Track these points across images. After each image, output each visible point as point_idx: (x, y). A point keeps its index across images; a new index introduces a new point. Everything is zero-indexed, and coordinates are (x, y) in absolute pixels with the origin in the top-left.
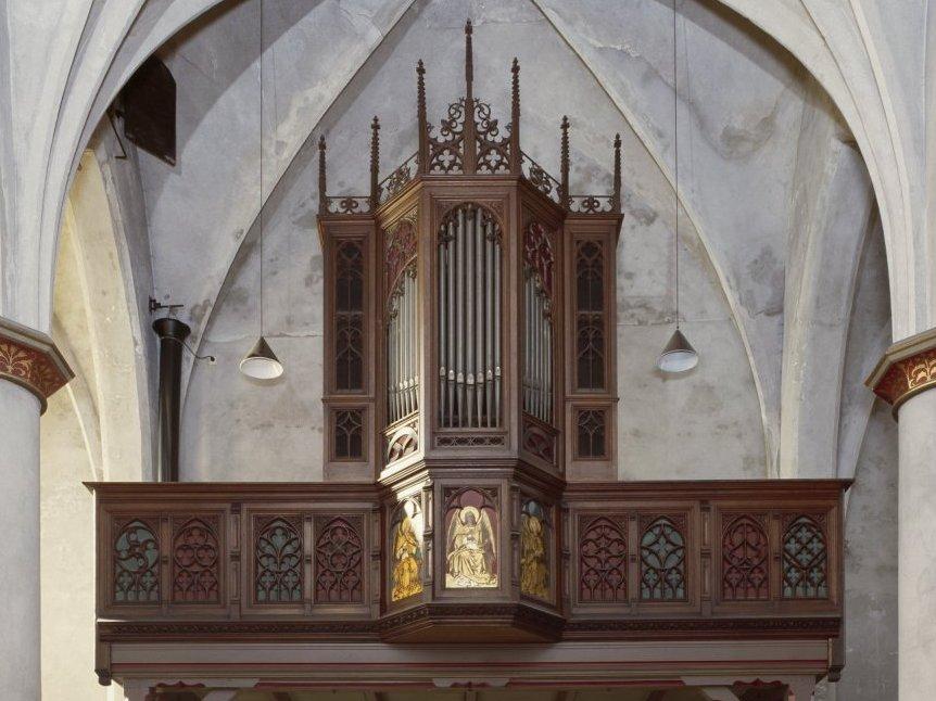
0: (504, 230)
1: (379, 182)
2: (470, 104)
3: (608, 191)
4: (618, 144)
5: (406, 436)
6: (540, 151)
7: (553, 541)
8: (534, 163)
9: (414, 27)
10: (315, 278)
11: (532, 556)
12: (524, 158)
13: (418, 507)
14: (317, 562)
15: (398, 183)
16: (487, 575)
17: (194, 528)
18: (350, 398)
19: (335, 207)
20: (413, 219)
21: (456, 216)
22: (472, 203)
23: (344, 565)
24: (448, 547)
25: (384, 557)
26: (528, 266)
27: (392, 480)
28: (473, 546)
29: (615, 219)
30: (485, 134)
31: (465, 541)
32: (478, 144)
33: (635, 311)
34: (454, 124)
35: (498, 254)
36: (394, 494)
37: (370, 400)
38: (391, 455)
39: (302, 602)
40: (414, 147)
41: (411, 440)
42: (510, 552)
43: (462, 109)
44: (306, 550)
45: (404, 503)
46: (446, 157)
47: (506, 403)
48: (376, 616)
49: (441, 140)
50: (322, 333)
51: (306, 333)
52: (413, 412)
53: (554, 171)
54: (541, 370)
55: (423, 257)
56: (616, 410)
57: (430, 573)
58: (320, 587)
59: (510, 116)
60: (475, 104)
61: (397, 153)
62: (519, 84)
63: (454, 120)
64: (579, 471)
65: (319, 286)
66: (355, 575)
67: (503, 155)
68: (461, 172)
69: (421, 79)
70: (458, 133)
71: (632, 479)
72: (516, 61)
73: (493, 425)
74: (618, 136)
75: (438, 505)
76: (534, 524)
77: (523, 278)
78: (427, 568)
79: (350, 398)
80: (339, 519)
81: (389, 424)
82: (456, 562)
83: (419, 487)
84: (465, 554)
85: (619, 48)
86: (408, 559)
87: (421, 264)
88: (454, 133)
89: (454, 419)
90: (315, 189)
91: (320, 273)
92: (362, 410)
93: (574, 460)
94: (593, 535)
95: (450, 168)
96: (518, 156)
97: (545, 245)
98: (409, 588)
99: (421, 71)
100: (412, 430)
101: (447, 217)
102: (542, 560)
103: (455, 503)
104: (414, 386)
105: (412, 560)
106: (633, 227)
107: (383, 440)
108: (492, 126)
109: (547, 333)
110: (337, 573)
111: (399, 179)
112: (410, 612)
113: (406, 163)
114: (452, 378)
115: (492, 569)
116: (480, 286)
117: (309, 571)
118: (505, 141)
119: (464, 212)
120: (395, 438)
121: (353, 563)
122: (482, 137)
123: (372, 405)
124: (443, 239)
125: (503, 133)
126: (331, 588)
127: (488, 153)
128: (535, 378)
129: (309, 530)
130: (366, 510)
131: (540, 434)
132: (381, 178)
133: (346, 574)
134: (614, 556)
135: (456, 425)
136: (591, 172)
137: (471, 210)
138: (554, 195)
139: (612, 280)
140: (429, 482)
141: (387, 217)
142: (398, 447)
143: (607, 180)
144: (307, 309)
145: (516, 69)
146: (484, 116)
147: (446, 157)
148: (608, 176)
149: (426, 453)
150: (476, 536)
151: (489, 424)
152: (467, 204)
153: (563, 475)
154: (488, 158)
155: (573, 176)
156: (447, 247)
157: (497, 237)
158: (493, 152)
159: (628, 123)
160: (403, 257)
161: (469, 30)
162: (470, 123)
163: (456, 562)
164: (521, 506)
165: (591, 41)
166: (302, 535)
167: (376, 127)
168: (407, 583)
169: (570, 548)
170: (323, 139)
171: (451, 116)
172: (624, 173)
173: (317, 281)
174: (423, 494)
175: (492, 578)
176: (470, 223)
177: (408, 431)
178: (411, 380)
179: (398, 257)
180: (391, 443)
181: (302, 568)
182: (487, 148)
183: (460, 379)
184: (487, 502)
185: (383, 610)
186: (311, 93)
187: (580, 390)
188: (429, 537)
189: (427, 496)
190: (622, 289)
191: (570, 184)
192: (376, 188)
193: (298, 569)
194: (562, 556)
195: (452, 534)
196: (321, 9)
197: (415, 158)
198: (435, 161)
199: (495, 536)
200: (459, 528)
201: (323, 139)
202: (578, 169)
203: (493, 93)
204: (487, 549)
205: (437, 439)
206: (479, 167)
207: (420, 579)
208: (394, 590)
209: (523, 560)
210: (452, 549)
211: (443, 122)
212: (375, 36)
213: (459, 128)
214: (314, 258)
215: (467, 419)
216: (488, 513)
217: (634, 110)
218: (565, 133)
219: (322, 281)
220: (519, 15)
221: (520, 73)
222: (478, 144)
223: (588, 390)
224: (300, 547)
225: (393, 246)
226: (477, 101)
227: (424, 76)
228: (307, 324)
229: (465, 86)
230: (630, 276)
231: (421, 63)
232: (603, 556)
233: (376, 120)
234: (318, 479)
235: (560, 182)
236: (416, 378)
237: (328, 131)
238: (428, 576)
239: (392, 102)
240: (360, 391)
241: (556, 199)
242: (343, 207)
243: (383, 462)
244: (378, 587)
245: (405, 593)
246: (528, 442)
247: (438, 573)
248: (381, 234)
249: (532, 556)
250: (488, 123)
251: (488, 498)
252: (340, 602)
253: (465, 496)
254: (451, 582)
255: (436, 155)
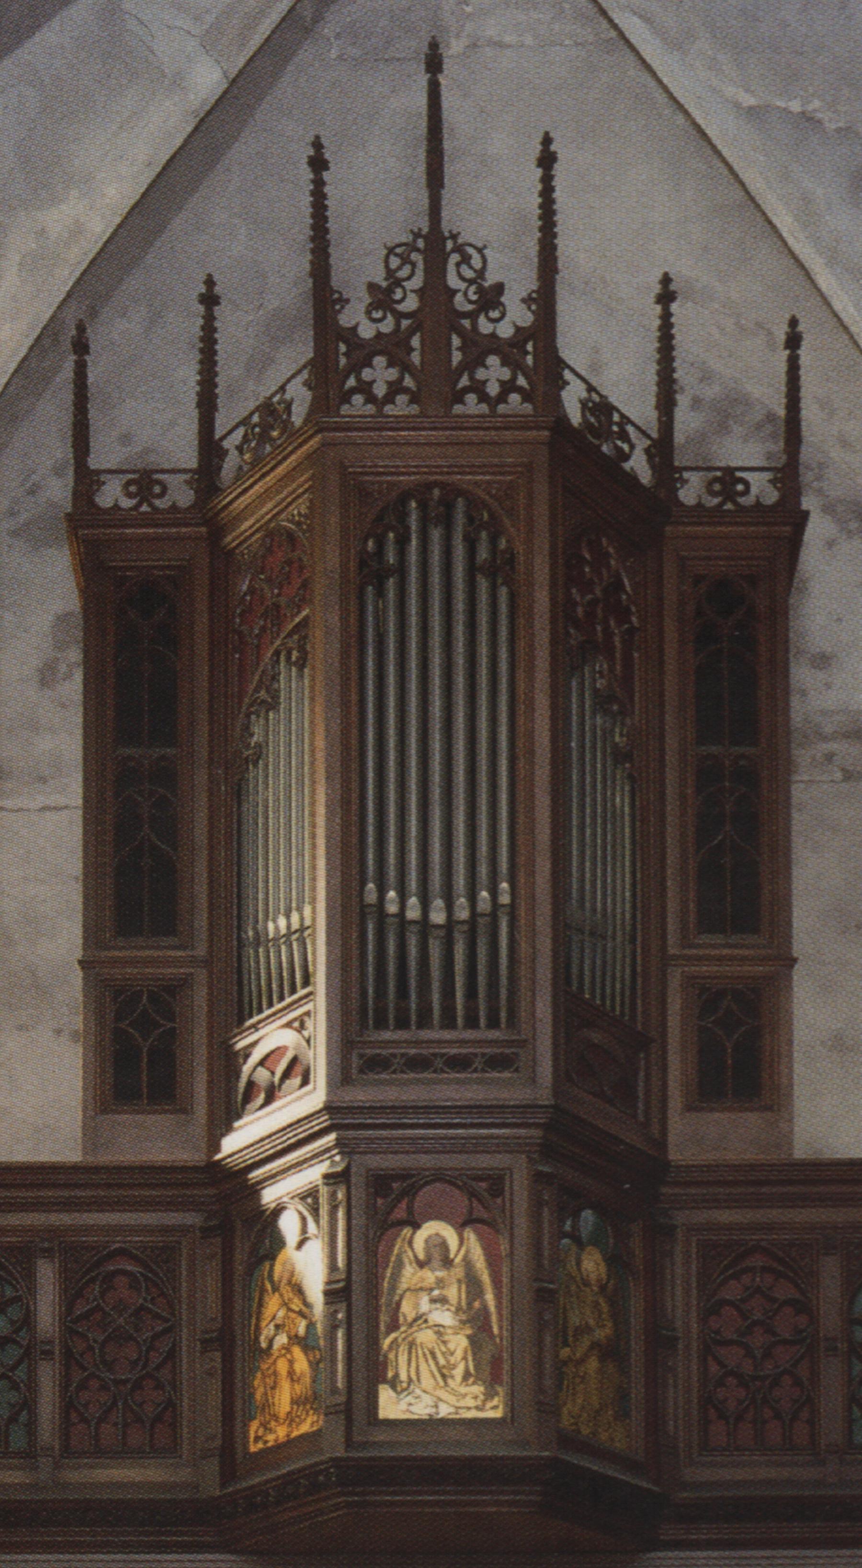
0: (520, 548)
1: (218, 435)
2: (435, 244)
3: (769, 456)
4: (793, 341)
5: (278, 1051)
6: (606, 357)
7: (636, 1305)
8: (591, 389)
9: (305, 54)
10: (63, 668)
11: (586, 1342)
12: (568, 375)
13: (312, 1227)
14: (68, 1354)
15: (264, 437)
16: (478, 1389)
17: (115, 1273)
18: (150, 959)
19: (111, 494)
20: (299, 524)
21: (403, 516)
22: (442, 485)
23: (135, 1363)
24: (384, 1319)
25: (234, 1347)
26: (575, 636)
27: (250, 1157)
28: (444, 1317)
29: (784, 525)
30: (473, 316)
31: (425, 1305)
32: (456, 341)
33: (833, 746)
34: (398, 295)
35: (503, 608)
36: (255, 1190)
37: (193, 961)
38: (248, 1097)
39: (29, 1455)
40: (302, 350)
41: (295, 1060)
42: (529, 1339)
43: (414, 256)
44: (40, 1327)
45: (279, 1210)
46: (380, 373)
47: (523, 971)
48: (212, 1488)
49: (367, 331)
50: (80, 802)
51: (41, 801)
52: (301, 992)
53: (636, 403)
54: (610, 887)
55: (324, 618)
56: (789, 988)
57: (340, 1384)
58: (74, 1417)
59: (534, 274)
60: (449, 245)
61: (259, 365)
62: (557, 195)
63: (398, 283)
64: (699, 1136)
65: (73, 687)
66: (159, 1386)
67: (516, 366)
68: (415, 409)
69: (319, 184)
70: (407, 315)
71: (828, 1155)
72: (547, 140)
73: (493, 1023)
74: (793, 322)
75: (359, 1221)
76: (592, 1264)
77: (567, 662)
78: (334, 1372)
79: (150, 959)
80: (122, 1252)
81: (241, 1020)
82: (403, 1359)
83: (314, 1174)
84: (426, 1337)
85: (795, 106)
86: (287, 1349)
87: (317, 634)
88: (399, 316)
89: (398, 1009)
90: (61, 450)
91: (75, 655)
92: (177, 988)
93: (689, 1108)
94: (732, 1291)
95: (389, 398)
96: (552, 369)
97: (619, 586)
98: (291, 1419)
99: (318, 163)
100: (293, 1035)
101: (379, 521)
102: (611, 1352)
103: (400, 1213)
104: (302, 929)
105: (297, 1352)
106: (830, 544)
107: (228, 1061)
108: (491, 298)
109: (622, 801)
110: (117, 1382)
111: (266, 428)
112: (290, 1478)
113: (282, 389)
114: (392, 908)
115: (489, 1370)
116: (460, 681)
117: (48, 1378)
118: (522, 335)
119: (423, 506)
120: (257, 1055)
121: (156, 1359)
122: (466, 323)
123: (201, 975)
124: (370, 573)
125: (516, 314)
126: (100, 1421)
127: (481, 362)
128: (594, 910)
129: (47, 1275)
130: (184, 1230)
131: (603, 1046)
132: (222, 423)
133: (138, 1385)
134: (785, 1342)
135: (402, 1023)
136: (727, 411)
137: (439, 502)
138: (638, 464)
139: (780, 670)
140: (339, 1163)
141: (239, 518)
142: (262, 1076)
143: (769, 428)
144: (45, 744)
145: (547, 160)
146: (469, 274)
147: (380, 373)
148: (770, 417)
149: (329, 1094)
150: (452, 1293)
151: (483, 1022)
152: (429, 486)
153: (661, 1144)
154: (481, 374)
155: (687, 421)
156: (380, 593)
157: (503, 568)
158: (493, 360)
159: (819, 290)
160: (276, 615)
161: (434, 63)
162: (435, 290)
163: (403, 1359)
164: (562, 1221)
165: (730, 91)
166: (32, 1290)
167: (210, 300)
168: (286, 1407)
169: (679, 1323)
170: (81, 328)
171: (390, 273)
172: (809, 412)
173: (68, 676)
174: (324, 1191)
175: (489, 1395)
176: (436, 534)
177: (287, 1038)
178: (295, 917)
179: (265, 616)
180: (246, 1069)
181: (32, 1373)
182: (479, 349)
183: (413, 913)
184: (480, 1212)
185: (229, 1473)
186: (56, 219)
187: (705, 939)
188: (335, 1294)
189: (333, 1195)
190: (804, 693)
191: (679, 437)
192: (210, 447)
193: (21, 1373)
194: (660, 1339)
195: (393, 1288)
196: (78, 17)
197: (305, 375)
198: (351, 382)
199: (498, 1297)
200: (410, 1275)
201: (81, 328)
202: (696, 403)
203: (491, 215)
204: (477, 1322)
205: (355, 1057)
206: (459, 397)
207: (316, 1396)
208: (254, 1426)
209: (565, 1352)
210: (394, 1326)
211: (372, 287)
212: (207, 80)
213: (411, 304)
214: (62, 619)
215: (430, 1010)
216: (481, 1237)
217: (833, 259)
218: (666, 318)
219: (78, 676)
220: (556, 27)
221: (559, 170)
222: (456, 341)
223: (719, 939)
224: (28, 1321)
225: (251, 591)
226: (454, 237)
227: (326, 175)
228: (43, 780)
229: (426, 201)
230: (822, 661)
231: (317, 145)
232: (758, 1340)
233: (210, 282)
234: (72, 1154)
235: (655, 435)
236: (307, 911)
237: (94, 313)
238: (334, 1391)
239: (247, 241)
240: (172, 940)
241: (645, 475)
242: (130, 495)
243: (227, 1112)
244: (215, 1414)
245: (281, 1432)
246: (575, 1063)
247: (359, 1377)
248: (223, 561)
249: (586, 1342)
250: (481, 291)
251: (479, 1203)
252: (123, 1452)
253: (426, 1194)
254: (391, 1406)
255: (355, 368)
